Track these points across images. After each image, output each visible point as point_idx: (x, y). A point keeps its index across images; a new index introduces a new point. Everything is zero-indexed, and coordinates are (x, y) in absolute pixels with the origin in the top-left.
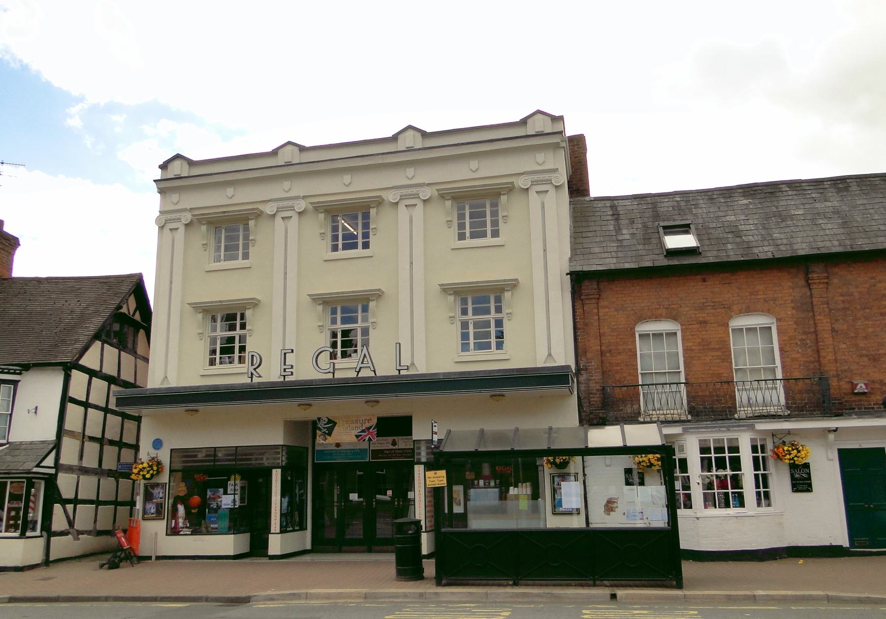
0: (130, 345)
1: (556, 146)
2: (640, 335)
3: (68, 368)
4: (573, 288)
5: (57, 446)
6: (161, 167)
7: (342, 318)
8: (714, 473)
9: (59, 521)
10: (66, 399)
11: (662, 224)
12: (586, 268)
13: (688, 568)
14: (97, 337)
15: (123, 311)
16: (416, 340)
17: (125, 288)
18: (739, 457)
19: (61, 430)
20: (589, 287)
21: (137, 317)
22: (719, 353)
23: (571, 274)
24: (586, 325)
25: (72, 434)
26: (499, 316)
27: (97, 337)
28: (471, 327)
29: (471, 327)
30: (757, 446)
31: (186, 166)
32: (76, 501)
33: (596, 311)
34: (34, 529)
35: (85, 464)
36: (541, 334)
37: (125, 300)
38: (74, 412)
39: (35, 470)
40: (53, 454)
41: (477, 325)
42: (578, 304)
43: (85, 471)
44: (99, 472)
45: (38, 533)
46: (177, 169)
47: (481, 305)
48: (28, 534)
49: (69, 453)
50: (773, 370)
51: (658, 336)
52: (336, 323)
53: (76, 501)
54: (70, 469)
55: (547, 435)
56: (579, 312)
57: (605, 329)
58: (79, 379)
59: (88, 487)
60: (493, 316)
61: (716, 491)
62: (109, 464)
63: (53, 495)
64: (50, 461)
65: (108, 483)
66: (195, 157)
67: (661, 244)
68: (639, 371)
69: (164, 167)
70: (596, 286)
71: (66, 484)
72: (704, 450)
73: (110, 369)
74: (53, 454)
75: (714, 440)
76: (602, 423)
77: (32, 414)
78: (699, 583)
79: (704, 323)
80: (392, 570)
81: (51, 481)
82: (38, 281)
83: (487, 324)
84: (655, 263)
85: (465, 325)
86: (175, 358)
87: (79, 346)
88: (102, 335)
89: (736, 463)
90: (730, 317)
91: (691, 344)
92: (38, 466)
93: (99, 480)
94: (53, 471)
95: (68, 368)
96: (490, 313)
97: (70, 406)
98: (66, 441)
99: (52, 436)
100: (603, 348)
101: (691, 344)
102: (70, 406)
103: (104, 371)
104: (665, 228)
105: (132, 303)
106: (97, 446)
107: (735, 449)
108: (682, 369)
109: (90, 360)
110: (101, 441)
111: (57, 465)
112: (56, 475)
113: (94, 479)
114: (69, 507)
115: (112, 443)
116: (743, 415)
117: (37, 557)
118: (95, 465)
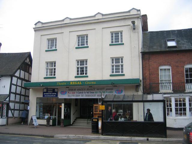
0: (27, 70)
1: (138, 18)
2: (160, 70)
3: (12, 76)
4: (142, 56)
5: (9, 96)
6: (35, 25)
7: (80, 64)
8: (182, 107)
9: (10, 114)
10: (11, 84)
11: (167, 39)
12: (153, 51)
13: (168, 132)
14: (19, 68)
15: (24, 62)
16: (100, 71)
17: (26, 55)
18: (185, 103)
19: (10, 92)
20: (147, 56)
21: (29, 63)
22: (181, 75)
23: (141, 52)
24: (145, 67)
25: (12, 93)
26: (122, 64)
27: (19, 68)
28: (114, 67)
29: (114, 67)
30: (190, 100)
31: (41, 24)
32: (14, 110)
33: (148, 63)
34: (4, 116)
35: (16, 100)
36: (133, 70)
37: (26, 59)
38: (14, 87)
39: (4, 101)
40: (8, 98)
41: (116, 66)
42: (144, 61)
43: (17, 102)
44: (19, 103)
45: (5, 117)
46: (39, 25)
47: (117, 62)
48: (3, 117)
49: (12, 97)
50: (170, 80)
51: (165, 70)
52: (113, 63)
53: (14, 110)
54: (12, 102)
55: (132, 97)
56: (144, 63)
57: (151, 68)
58: (15, 79)
59: (17, 106)
60: (85, 66)
61: (182, 112)
62: (22, 100)
63: (8, 108)
64: (8, 99)
65: (22, 106)
66: (44, 22)
67: (166, 44)
68: (160, 79)
69: (36, 24)
70: (148, 56)
71: (12, 105)
72: (176, 101)
73: (22, 76)
74: (8, 98)
75: (183, 98)
76: (149, 94)
77: (3, 88)
78: (171, 136)
79: (177, 66)
80: (91, 130)
81: (8, 105)
82: (6, 54)
83: (119, 66)
84: (159, 48)
85: (113, 66)
86: (38, 74)
87: (14, 71)
88: (20, 68)
89: (184, 105)
90: (185, 65)
91: (174, 72)
92: (5, 101)
93: (15, 104)
94: (8, 102)
95: (12, 76)
96: (120, 63)
97: (12, 86)
98: (12, 95)
99: (8, 93)
100: (150, 73)
101: (174, 72)
102: (12, 86)
103: (21, 77)
104: (167, 40)
105: (28, 60)
106: (19, 96)
107: (184, 100)
108: (171, 79)
109: (17, 74)
110: (20, 95)
111: (9, 101)
112: (9, 103)
113: (18, 105)
114: (13, 111)
115: (23, 95)
116: (187, 92)
117: (5, 123)
118: (19, 101)
